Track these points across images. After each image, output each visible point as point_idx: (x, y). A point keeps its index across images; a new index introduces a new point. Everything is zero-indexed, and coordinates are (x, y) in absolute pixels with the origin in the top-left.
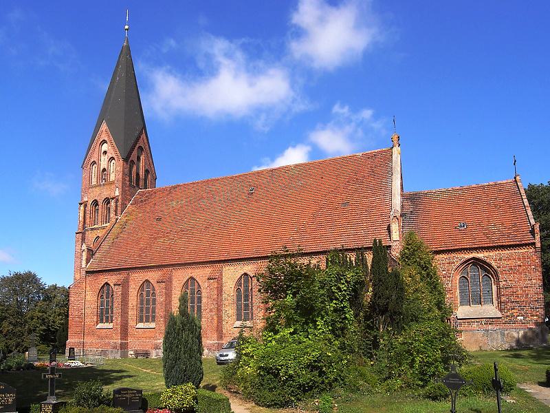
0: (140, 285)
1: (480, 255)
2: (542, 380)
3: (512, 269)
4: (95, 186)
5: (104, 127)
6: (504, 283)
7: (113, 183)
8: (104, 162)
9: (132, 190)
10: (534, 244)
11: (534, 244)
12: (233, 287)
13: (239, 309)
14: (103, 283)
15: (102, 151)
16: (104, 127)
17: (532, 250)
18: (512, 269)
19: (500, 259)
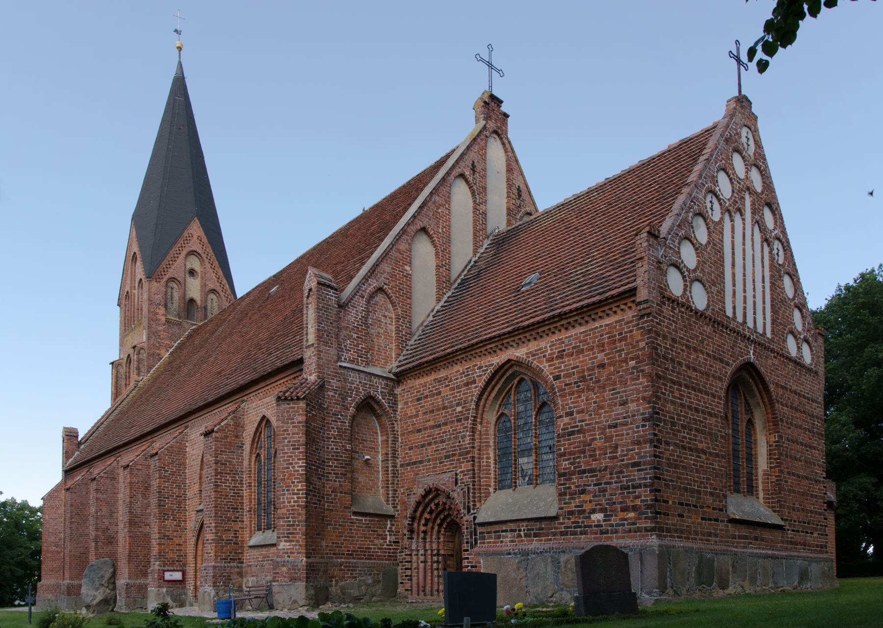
6: (566, 420)
9: (176, 329)
18: (583, 379)
19: (560, 356)
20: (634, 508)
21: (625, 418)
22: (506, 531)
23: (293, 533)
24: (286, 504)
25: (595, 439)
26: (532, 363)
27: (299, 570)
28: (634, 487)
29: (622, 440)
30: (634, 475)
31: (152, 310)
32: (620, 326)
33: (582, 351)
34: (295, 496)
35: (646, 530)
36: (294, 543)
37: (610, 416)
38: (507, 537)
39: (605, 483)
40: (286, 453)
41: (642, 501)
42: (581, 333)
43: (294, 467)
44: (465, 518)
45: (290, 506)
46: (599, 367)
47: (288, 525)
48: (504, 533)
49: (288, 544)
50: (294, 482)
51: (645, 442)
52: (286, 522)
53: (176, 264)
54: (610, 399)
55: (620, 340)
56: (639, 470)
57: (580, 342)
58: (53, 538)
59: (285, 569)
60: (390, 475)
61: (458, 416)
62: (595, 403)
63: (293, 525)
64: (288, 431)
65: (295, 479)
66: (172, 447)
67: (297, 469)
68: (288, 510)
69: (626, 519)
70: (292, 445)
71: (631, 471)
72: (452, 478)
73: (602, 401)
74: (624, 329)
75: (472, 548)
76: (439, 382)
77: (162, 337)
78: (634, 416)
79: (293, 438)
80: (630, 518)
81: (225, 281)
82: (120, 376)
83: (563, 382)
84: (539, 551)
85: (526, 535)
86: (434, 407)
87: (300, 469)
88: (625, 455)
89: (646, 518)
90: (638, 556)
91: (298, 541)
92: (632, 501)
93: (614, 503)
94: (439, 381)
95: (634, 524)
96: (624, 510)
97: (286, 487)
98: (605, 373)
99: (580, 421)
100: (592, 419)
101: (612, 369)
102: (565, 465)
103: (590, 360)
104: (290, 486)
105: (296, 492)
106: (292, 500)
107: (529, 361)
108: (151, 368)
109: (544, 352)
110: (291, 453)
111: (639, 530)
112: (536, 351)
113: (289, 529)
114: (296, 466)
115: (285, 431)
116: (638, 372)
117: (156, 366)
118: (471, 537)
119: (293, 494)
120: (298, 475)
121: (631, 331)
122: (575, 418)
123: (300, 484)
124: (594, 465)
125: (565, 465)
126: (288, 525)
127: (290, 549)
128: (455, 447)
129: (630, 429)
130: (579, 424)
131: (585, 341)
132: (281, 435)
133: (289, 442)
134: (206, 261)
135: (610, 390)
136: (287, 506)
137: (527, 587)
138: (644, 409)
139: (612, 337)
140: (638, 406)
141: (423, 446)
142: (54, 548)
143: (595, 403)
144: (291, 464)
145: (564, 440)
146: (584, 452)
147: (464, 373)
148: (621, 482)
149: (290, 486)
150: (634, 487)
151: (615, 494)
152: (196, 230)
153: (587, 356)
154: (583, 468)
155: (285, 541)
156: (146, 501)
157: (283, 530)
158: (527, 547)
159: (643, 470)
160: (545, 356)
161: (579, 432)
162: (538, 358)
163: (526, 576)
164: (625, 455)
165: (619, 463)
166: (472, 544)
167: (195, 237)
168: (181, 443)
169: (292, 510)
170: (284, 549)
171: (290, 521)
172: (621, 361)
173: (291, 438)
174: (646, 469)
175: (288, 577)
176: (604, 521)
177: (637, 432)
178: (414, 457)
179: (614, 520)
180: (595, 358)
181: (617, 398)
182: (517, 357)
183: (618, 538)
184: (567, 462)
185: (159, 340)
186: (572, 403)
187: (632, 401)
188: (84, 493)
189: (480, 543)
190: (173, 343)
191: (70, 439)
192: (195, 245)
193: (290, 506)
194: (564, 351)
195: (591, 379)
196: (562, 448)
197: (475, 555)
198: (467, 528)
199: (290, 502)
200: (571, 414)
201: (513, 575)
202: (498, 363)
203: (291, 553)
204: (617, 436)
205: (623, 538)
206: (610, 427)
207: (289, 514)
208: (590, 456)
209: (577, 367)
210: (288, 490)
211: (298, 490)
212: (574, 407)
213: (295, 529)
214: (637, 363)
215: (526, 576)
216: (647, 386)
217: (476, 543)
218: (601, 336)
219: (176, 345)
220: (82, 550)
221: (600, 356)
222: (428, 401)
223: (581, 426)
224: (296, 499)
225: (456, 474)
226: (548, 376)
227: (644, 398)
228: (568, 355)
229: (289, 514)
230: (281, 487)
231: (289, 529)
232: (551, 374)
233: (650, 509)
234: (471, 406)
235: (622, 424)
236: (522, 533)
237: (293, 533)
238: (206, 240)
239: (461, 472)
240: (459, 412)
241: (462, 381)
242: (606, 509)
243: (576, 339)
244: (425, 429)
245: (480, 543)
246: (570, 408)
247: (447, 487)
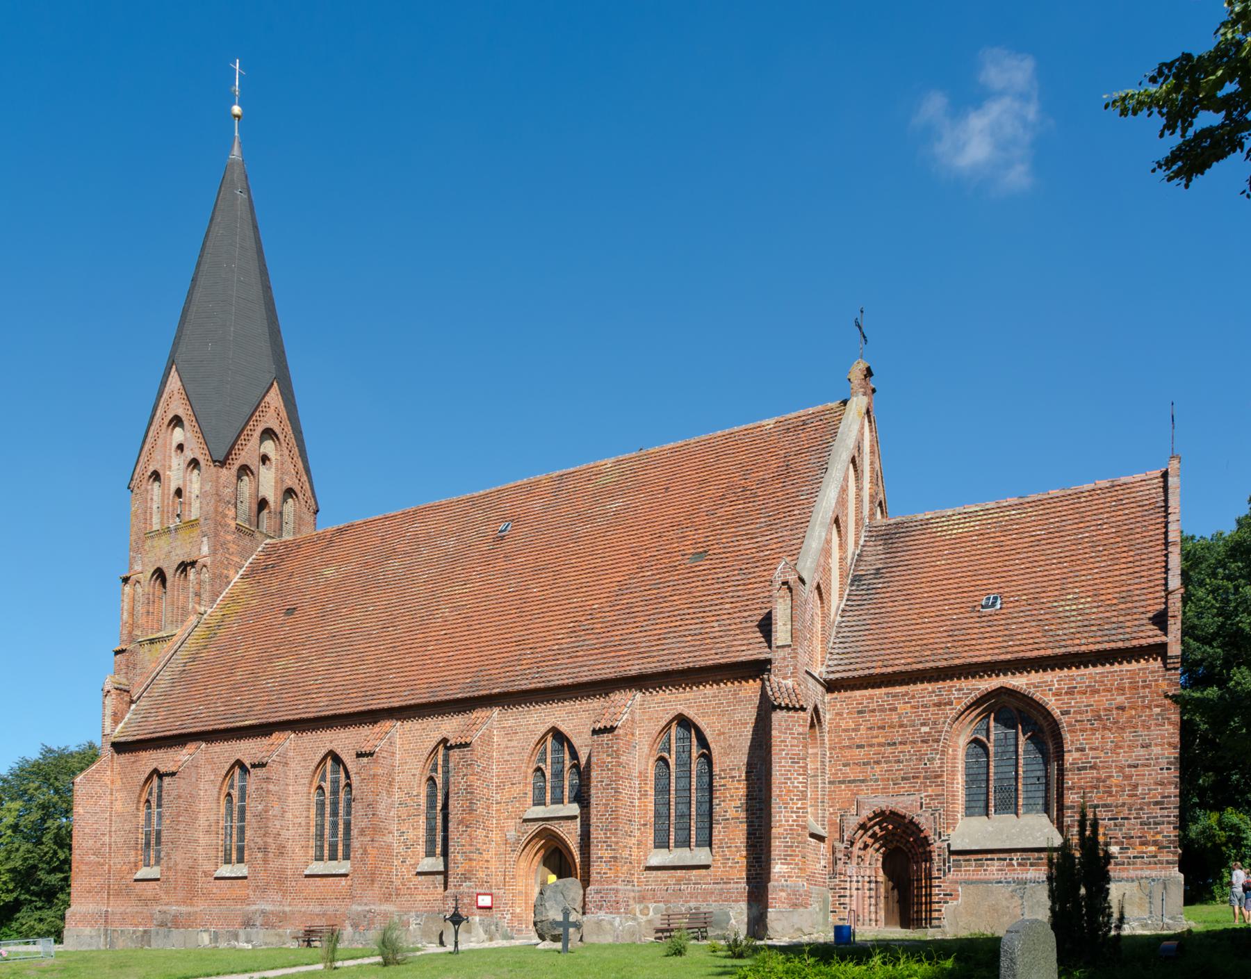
0: (224, 772)
1: (1018, 681)
2: (1184, 182)
3: (1099, 718)
4: (159, 533)
5: (174, 382)
6: (1076, 755)
7: (192, 524)
8: (175, 473)
9: (246, 541)
10: (1164, 646)
11: (1164, 646)
12: (417, 772)
13: (661, 815)
14: (148, 771)
15: (174, 445)
16: (174, 382)
17: (1156, 664)
18: (1099, 718)
19: (1070, 692)
20: (1155, 843)
21: (1148, 759)
22: (992, 859)
23: (791, 855)
24: (783, 822)
25: (1113, 777)
26: (1034, 694)
27: (801, 895)
28: (1156, 823)
29: (1144, 779)
30: (1156, 813)
31: (220, 510)
32: (1144, 673)
33: (1097, 691)
34: (794, 815)
35: (1168, 862)
36: (792, 866)
37: (1131, 757)
38: (993, 866)
39: (1122, 819)
40: (784, 766)
41: (1163, 837)
42: (1097, 674)
43: (793, 783)
44: (936, 845)
45: (788, 825)
46: (1117, 708)
47: (785, 846)
48: (989, 862)
49: (786, 867)
50: (793, 799)
51: (1170, 783)
52: (783, 842)
53: (250, 445)
54: (1130, 741)
55: (1144, 687)
56: (1161, 809)
57: (1095, 682)
58: (91, 842)
59: (783, 894)
60: (819, 793)
61: (924, 737)
62: (1112, 742)
63: (792, 847)
64: (786, 742)
65: (794, 795)
66: (484, 736)
67: (796, 784)
68: (786, 830)
69: (1145, 853)
70: (790, 758)
71: (1153, 809)
72: (916, 802)
73: (1121, 741)
74: (1148, 677)
75: (944, 875)
76: (894, 696)
77: (231, 550)
78: (1158, 758)
79: (792, 750)
80: (1150, 852)
81: (304, 478)
82: (965, 707)
83: (1073, 718)
84: (1040, 880)
85: (1019, 864)
86: (885, 723)
87: (800, 785)
88: (1146, 794)
89: (1168, 852)
90: (1161, 886)
91: (797, 864)
92: (1153, 836)
93: (1132, 837)
94: (895, 696)
95: (1156, 856)
96: (1142, 844)
97: (783, 804)
98: (1126, 715)
99: (1092, 758)
100: (1109, 757)
101: (1133, 712)
102: (1073, 798)
103: (1107, 700)
104: (789, 804)
105: (795, 810)
106: (791, 819)
107: (1029, 692)
108: (218, 596)
109: (1049, 685)
110: (789, 766)
111: (1161, 862)
112: (1039, 683)
113: (787, 851)
114: (796, 781)
115: (782, 741)
116: (1163, 719)
117: (224, 594)
118: (944, 865)
119: (792, 812)
120: (798, 791)
121: (1156, 681)
122: (1088, 755)
123: (800, 802)
124: (1109, 800)
125: (1073, 798)
126: (785, 846)
127: (788, 872)
128: (918, 769)
129: (1153, 770)
130: (1093, 760)
131: (1103, 682)
132: (777, 745)
133: (787, 754)
134: (284, 445)
135: (1130, 732)
136: (785, 825)
137: (1023, 915)
138: (1169, 753)
139: (1135, 682)
140: (1162, 750)
141: (867, 764)
142: (93, 857)
143: (1112, 742)
144: (790, 779)
145: (1073, 774)
146: (1097, 787)
147: (934, 692)
148: (1141, 818)
149: (789, 804)
150: (1156, 823)
151: (1134, 829)
152: (274, 398)
153: (1104, 696)
154: (1096, 802)
155: (782, 863)
156: (389, 801)
157: (779, 851)
158: (1020, 876)
159: (1166, 808)
160: (1050, 690)
161: (1091, 768)
162: (1042, 691)
163: (1022, 904)
164: (1146, 794)
165: (1139, 801)
166: (944, 872)
167: (272, 408)
168: (490, 731)
169: (791, 830)
170: (780, 872)
171: (788, 842)
172: (1144, 707)
173: (789, 750)
174: (1170, 808)
175: (788, 903)
176: (1120, 853)
177: (1162, 774)
178: (852, 775)
179: (1131, 853)
180: (1115, 699)
181: (1138, 740)
182: (1014, 686)
183: (1134, 869)
184: (1076, 796)
185: (227, 556)
186: (1084, 739)
187: (1156, 745)
188: (194, 780)
189: (954, 871)
190: (243, 562)
191: (119, 695)
192: (270, 421)
193: (788, 825)
194: (1076, 687)
195: (1107, 719)
196: (1070, 782)
197: (951, 883)
198: (939, 855)
199: (788, 821)
200: (1083, 750)
201: (1005, 903)
202: (986, 689)
203: (789, 877)
204: (1137, 775)
205: (1142, 869)
206: (1130, 766)
207: (787, 834)
208: (1105, 792)
209: (1092, 705)
210: (785, 808)
211: (797, 808)
212: (1086, 744)
213: (794, 851)
214: (1161, 710)
215: (1022, 904)
216: (1174, 733)
217: (949, 871)
218: (1121, 680)
219: (247, 564)
220: (190, 862)
221: (1120, 699)
222: (876, 716)
223: (1095, 763)
224: (795, 818)
225: (921, 798)
226: (1053, 709)
227: (1169, 744)
228: (1079, 692)
229: (787, 834)
230: (777, 804)
231: (787, 851)
232: (1058, 708)
233: (1173, 844)
234: (943, 728)
235: (1143, 765)
236: (1015, 862)
237: (791, 855)
238: (285, 414)
239: (926, 796)
240: (925, 733)
241: (930, 701)
242: (1123, 842)
243: (1091, 678)
244: (871, 746)
245: (954, 871)
246: (1081, 744)
247: (910, 811)
